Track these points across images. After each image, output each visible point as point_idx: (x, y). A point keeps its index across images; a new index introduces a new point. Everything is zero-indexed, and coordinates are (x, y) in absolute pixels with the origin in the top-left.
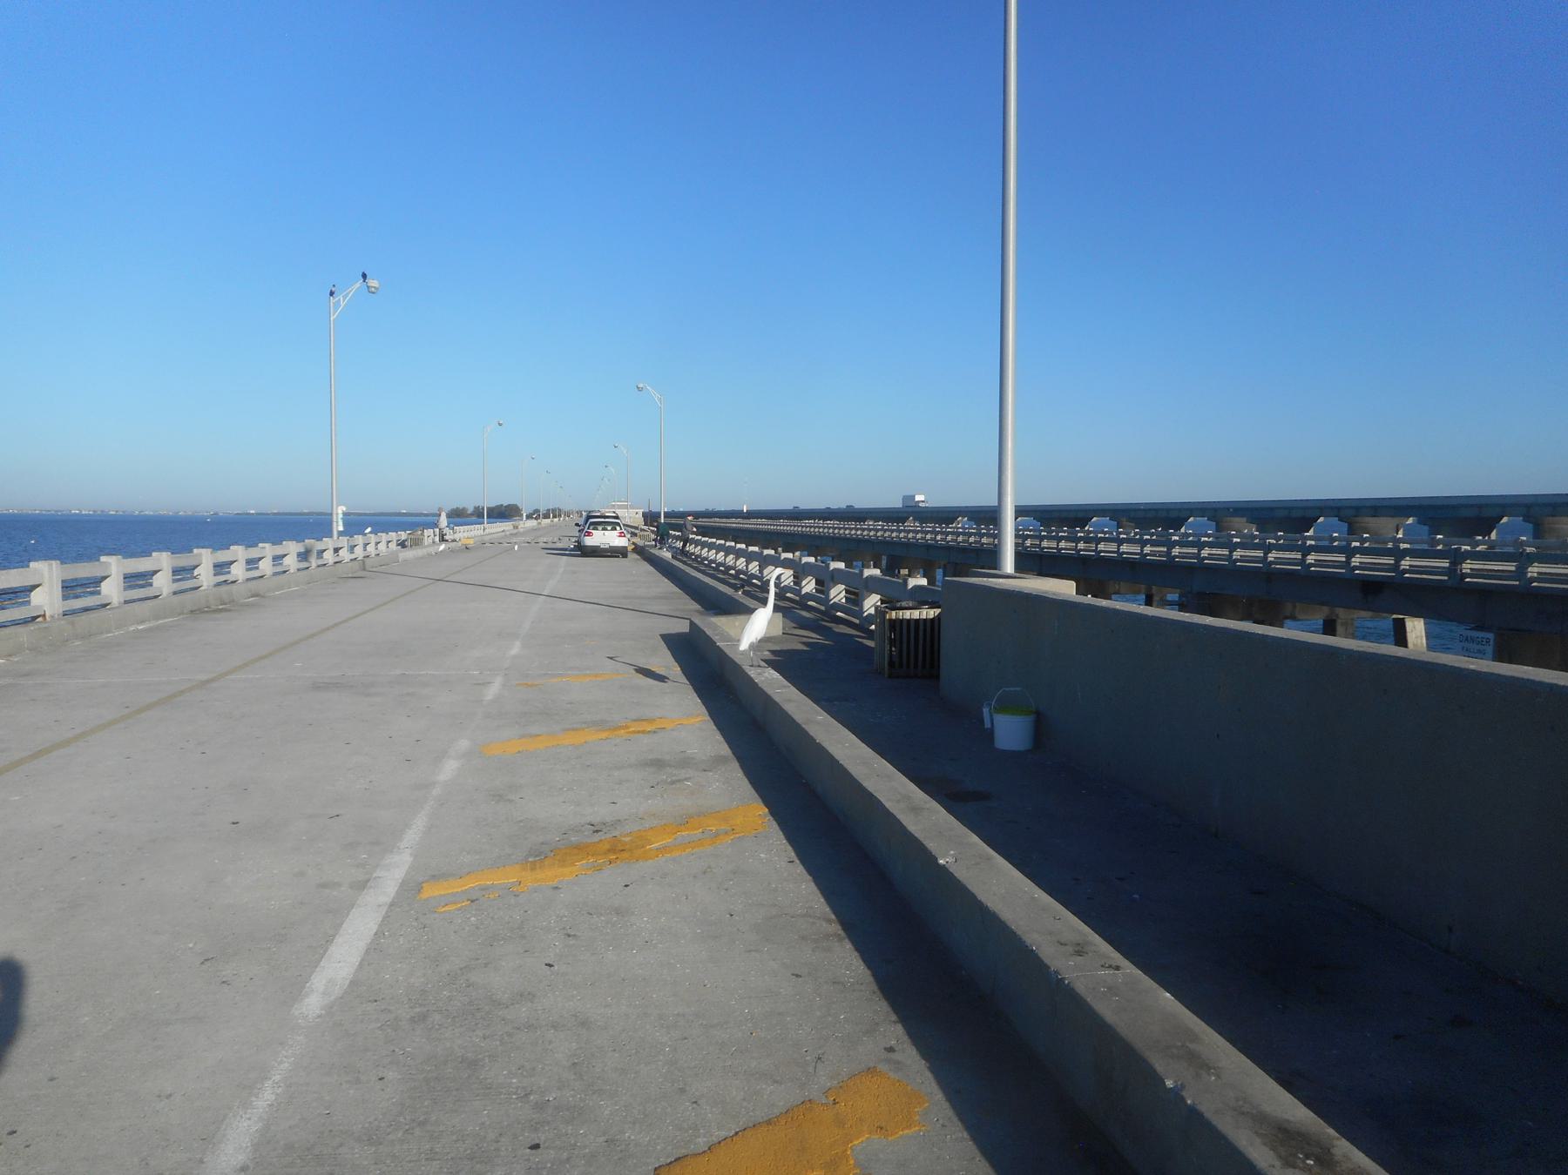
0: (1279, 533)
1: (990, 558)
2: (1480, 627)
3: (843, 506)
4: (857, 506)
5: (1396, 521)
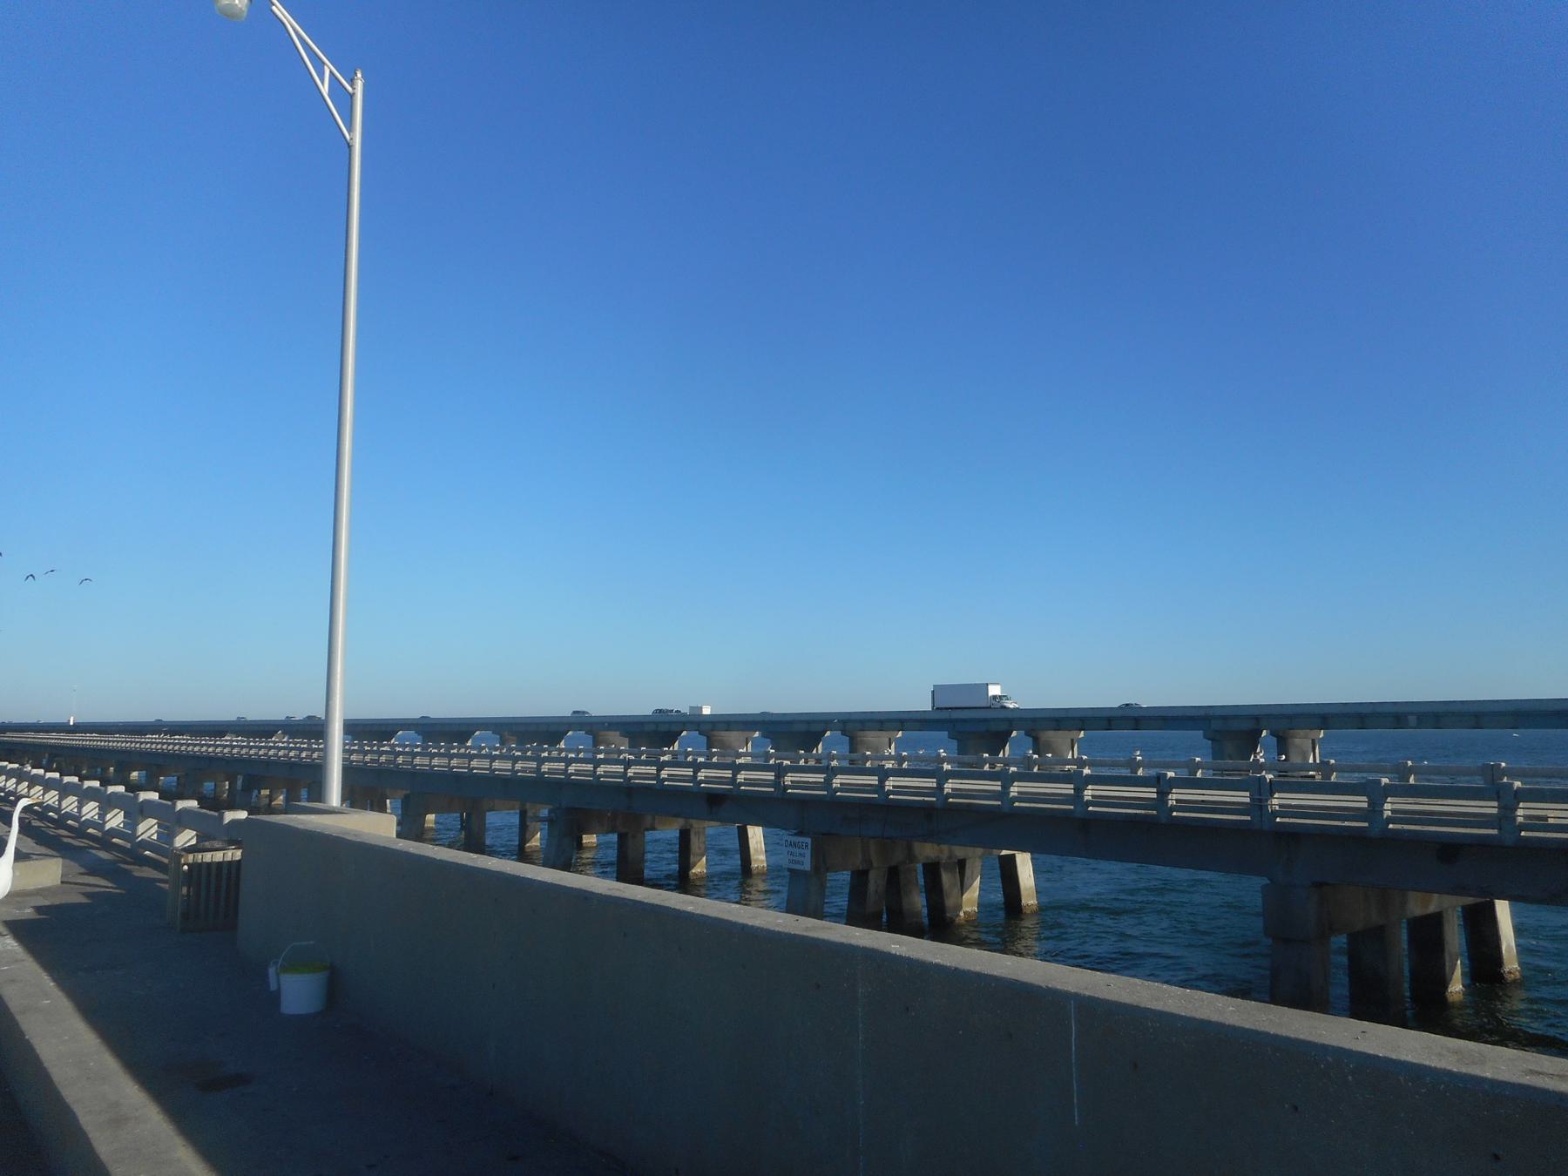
0: (642, 748)
1: (308, 779)
2: (800, 834)
3: (234, 718)
4: (164, 720)
5: (747, 734)
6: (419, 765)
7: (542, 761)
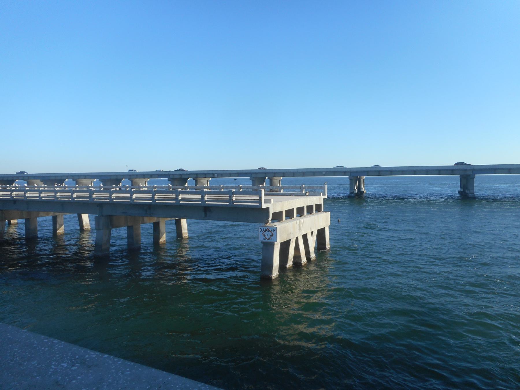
0: (7, 185)
5: (91, 180)
6: (44, 197)
7: (111, 193)
